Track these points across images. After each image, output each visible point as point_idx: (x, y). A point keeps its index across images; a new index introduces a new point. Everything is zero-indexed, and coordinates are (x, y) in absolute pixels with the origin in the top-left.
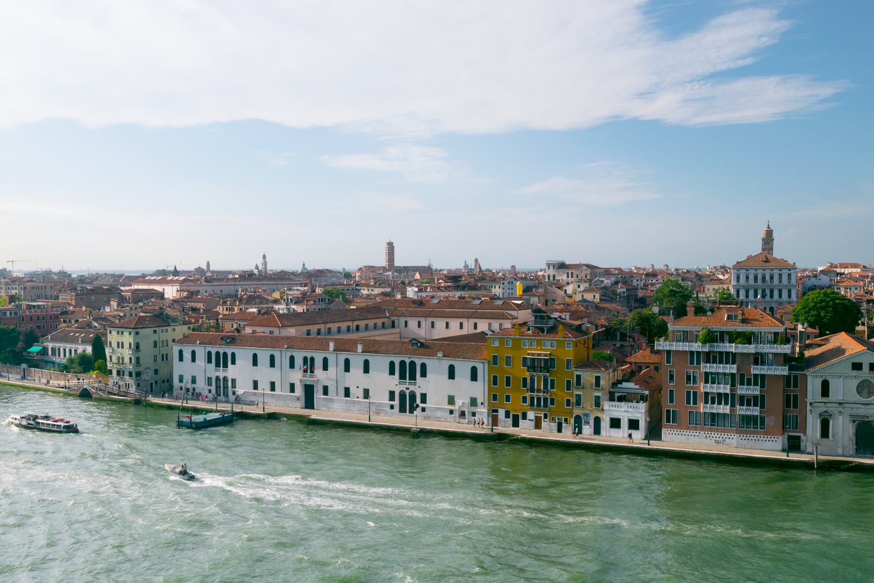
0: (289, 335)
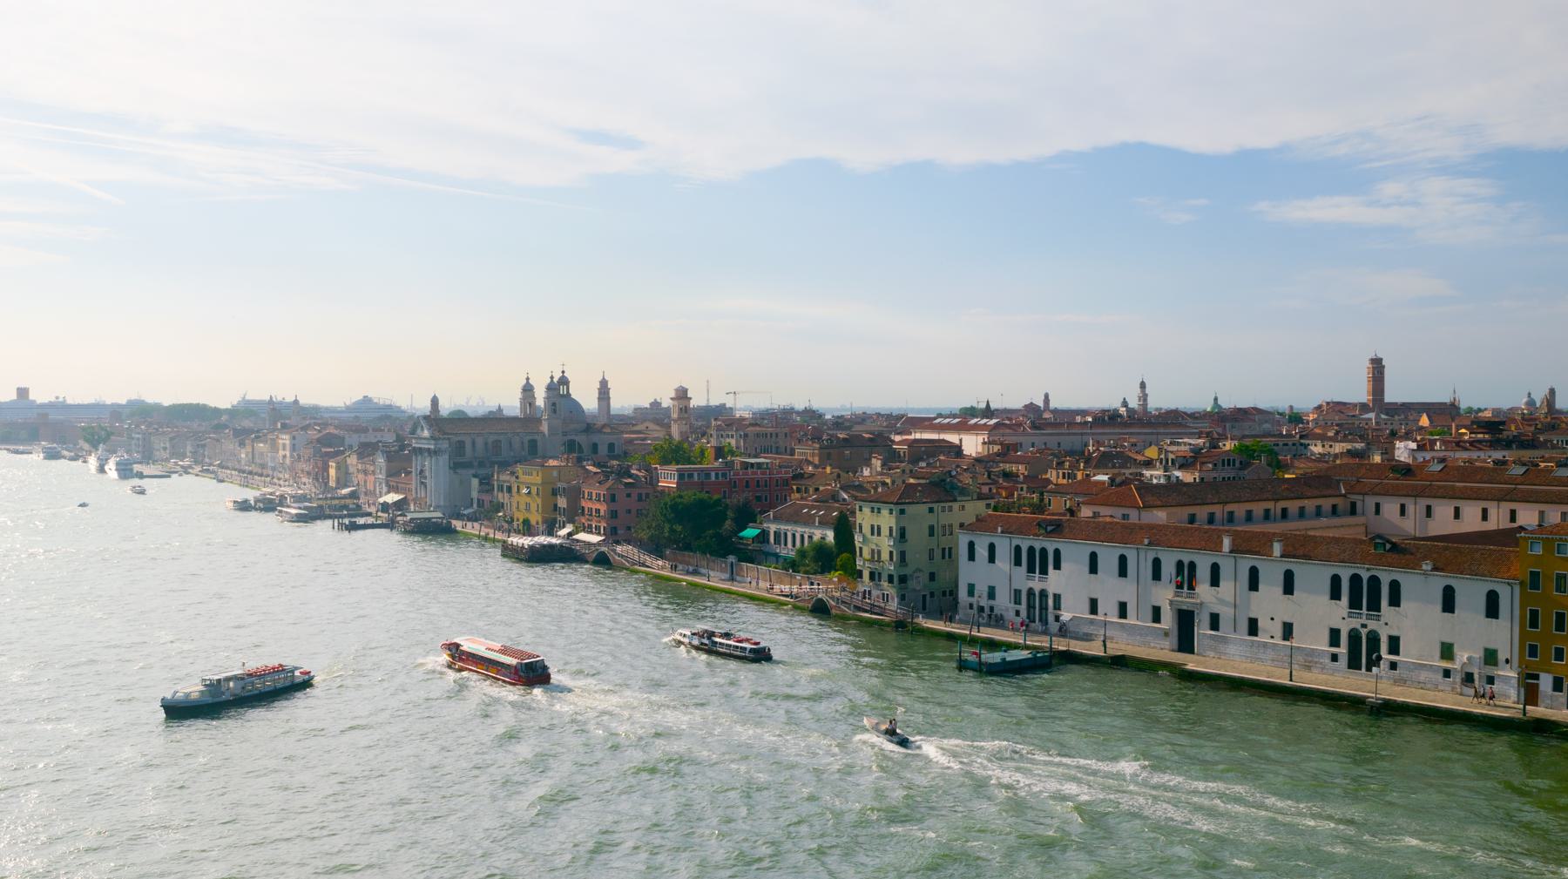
0: (1154, 521)
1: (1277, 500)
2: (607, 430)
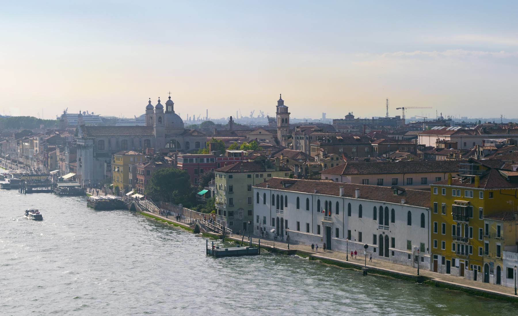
1: (404, 173)
2: (196, 134)
